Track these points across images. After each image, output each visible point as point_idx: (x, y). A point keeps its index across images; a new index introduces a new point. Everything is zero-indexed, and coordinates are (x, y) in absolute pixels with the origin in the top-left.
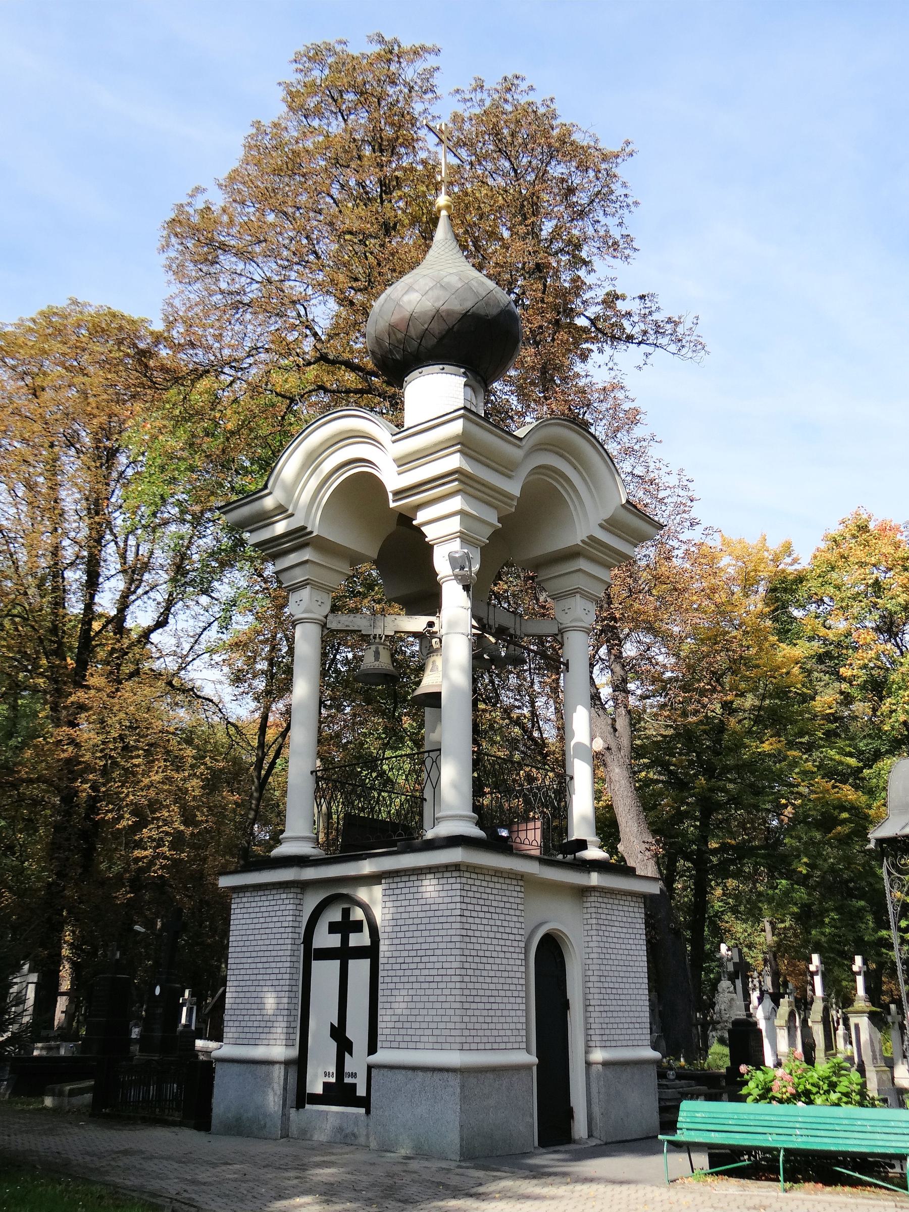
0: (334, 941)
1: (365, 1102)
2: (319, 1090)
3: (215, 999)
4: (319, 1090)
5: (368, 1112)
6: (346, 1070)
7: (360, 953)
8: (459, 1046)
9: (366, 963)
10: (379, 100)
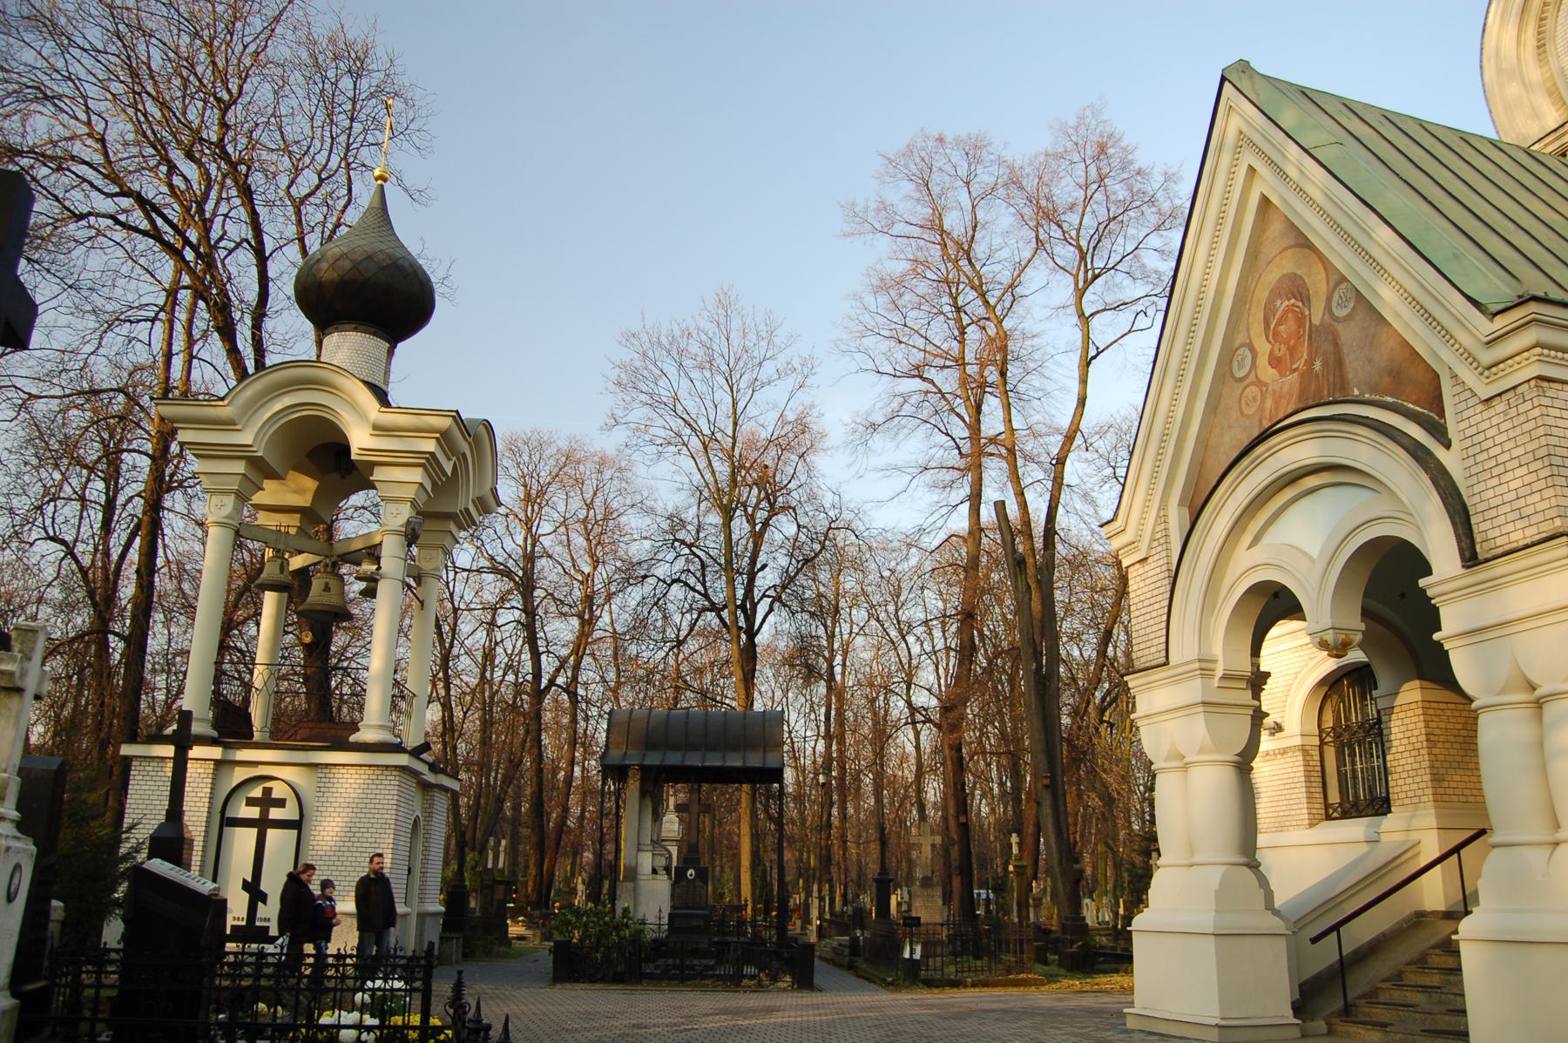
0: (254, 812)
6: (258, 916)
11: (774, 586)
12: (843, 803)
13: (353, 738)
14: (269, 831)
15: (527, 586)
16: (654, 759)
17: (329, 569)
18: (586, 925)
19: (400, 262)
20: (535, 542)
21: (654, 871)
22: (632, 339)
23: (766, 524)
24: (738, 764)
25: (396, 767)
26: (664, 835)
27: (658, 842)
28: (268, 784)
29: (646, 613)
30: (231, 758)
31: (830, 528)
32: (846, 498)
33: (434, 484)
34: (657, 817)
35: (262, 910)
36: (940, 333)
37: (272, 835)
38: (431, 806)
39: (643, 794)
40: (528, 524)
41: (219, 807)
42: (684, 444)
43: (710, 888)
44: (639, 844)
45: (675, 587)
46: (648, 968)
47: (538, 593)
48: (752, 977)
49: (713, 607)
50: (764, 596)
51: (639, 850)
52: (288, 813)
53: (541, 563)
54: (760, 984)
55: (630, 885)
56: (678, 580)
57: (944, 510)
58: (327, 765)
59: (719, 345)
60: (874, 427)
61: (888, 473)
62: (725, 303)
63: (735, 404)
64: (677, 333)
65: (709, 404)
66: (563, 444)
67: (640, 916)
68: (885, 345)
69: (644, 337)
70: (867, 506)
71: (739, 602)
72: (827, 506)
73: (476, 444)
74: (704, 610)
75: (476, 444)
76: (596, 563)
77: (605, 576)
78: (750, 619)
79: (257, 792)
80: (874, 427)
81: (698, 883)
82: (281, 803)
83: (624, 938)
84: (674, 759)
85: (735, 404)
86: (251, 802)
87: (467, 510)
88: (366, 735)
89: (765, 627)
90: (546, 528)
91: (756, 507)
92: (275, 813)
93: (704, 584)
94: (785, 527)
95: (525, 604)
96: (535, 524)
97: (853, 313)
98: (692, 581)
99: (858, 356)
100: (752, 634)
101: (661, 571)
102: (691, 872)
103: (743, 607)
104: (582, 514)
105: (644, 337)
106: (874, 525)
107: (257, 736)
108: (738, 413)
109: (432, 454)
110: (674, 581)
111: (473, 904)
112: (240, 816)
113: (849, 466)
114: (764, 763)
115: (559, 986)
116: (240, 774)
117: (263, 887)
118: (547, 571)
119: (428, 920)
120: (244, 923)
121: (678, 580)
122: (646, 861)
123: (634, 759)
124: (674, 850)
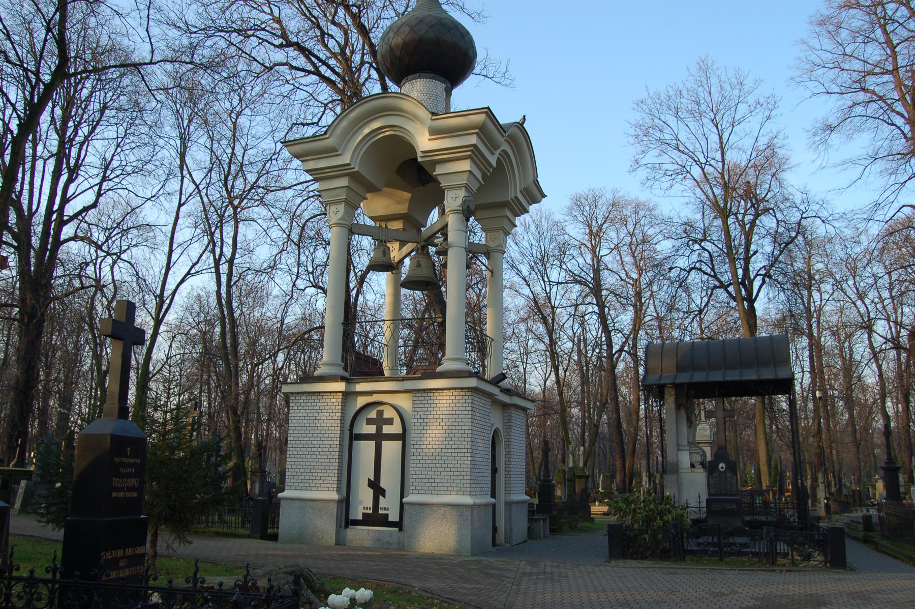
0: (371, 429)
1: (399, 525)
2: (360, 517)
3: (587, 445)
4: (360, 517)
5: (401, 530)
6: (380, 506)
7: (392, 437)
8: (469, 493)
9: (398, 444)
10: (316, 286)
11: (764, 266)
12: (827, 420)
13: (439, 369)
14: (384, 442)
15: (596, 289)
16: (684, 378)
17: (419, 252)
18: (635, 511)
19: (444, 21)
20: (599, 262)
21: (692, 466)
22: (640, 104)
23: (753, 223)
24: (754, 377)
25: (468, 388)
26: (698, 439)
27: (693, 444)
28: (380, 408)
29: (674, 293)
30: (353, 390)
31: (802, 218)
32: (811, 195)
33: (484, 176)
34: (691, 424)
35: (383, 502)
36: (875, 53)
37: (387, 445)
38: (510, 420)
39: (678, 407)
40: (593, 251)
41: (347, 426)
42: (688, 172)
43: (739, 476)
44: (678, 445)
45: (693, 273)
46: (692, 545)
47: (604, 293)
48: (785, 555)
49: (722, 286)
50: (757, 275)
51: (678, 450)
52: (395, 428)
53: (605, 274)
54: (794, 563)
55: (673, 477)
56: (694, 268)
57: (897, 186)
58: (431, 390)
59: (703, 94)
60: (831, 128)
61: (845, 166)
62: (705, 69)
63: (721, 137)
64: (671, 93)
65: (700, 137)
66: (609, 196)
67: (683, 503)
68: (831, 74)
69: (649, 102)
70: (829, 197)
71: (740, 280)
72: (798, 202)
73: (513, 141)
74: (715, 287)
75: (513, 141)
76: (640, 271)
77: (647, 279)
78: (749, 291)
79: (373, 414)
80: (831, 128)
81: (729, 474)
82: (390, 421)
83: (668, 522)
84: (699, 377)
85: (721, 137)
86: (370, 422)
87: (516, 198)
88: (447, 365)
89: (761, 294)
90: (604, 252)
91: (744, 214)
92: (387, 429)
93: (713, 269)
94: (768, 222)
95: (597, 301)
96: (598, 250)
97: (802, 55)
98: (704, 268)
99: (810, 84)
100: (751, 302)
101: (682, 263)
102: (722, 465)
103: (743, 283)
104: (628, 240)
105: (649, 102)
106: (836, 211)
107: (387, 373)
108: (724, 141)
109: (474, 146)
110: (691, 269)
111: (559, 493)
112: (363, 432)
113: (813, 161)
114: (776, 375)
115: (613, 563)
116: (361, 401)
117: (382, 485)
118: (609, 280)
119: (514, 507)
120: (371, 512)
121: (694, 268)
122: (685, 458)
123: (667, 379)
124: (708, 450)
